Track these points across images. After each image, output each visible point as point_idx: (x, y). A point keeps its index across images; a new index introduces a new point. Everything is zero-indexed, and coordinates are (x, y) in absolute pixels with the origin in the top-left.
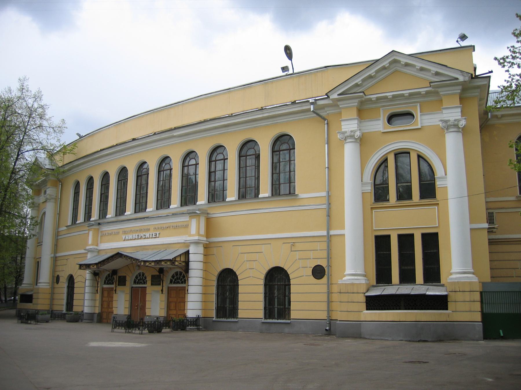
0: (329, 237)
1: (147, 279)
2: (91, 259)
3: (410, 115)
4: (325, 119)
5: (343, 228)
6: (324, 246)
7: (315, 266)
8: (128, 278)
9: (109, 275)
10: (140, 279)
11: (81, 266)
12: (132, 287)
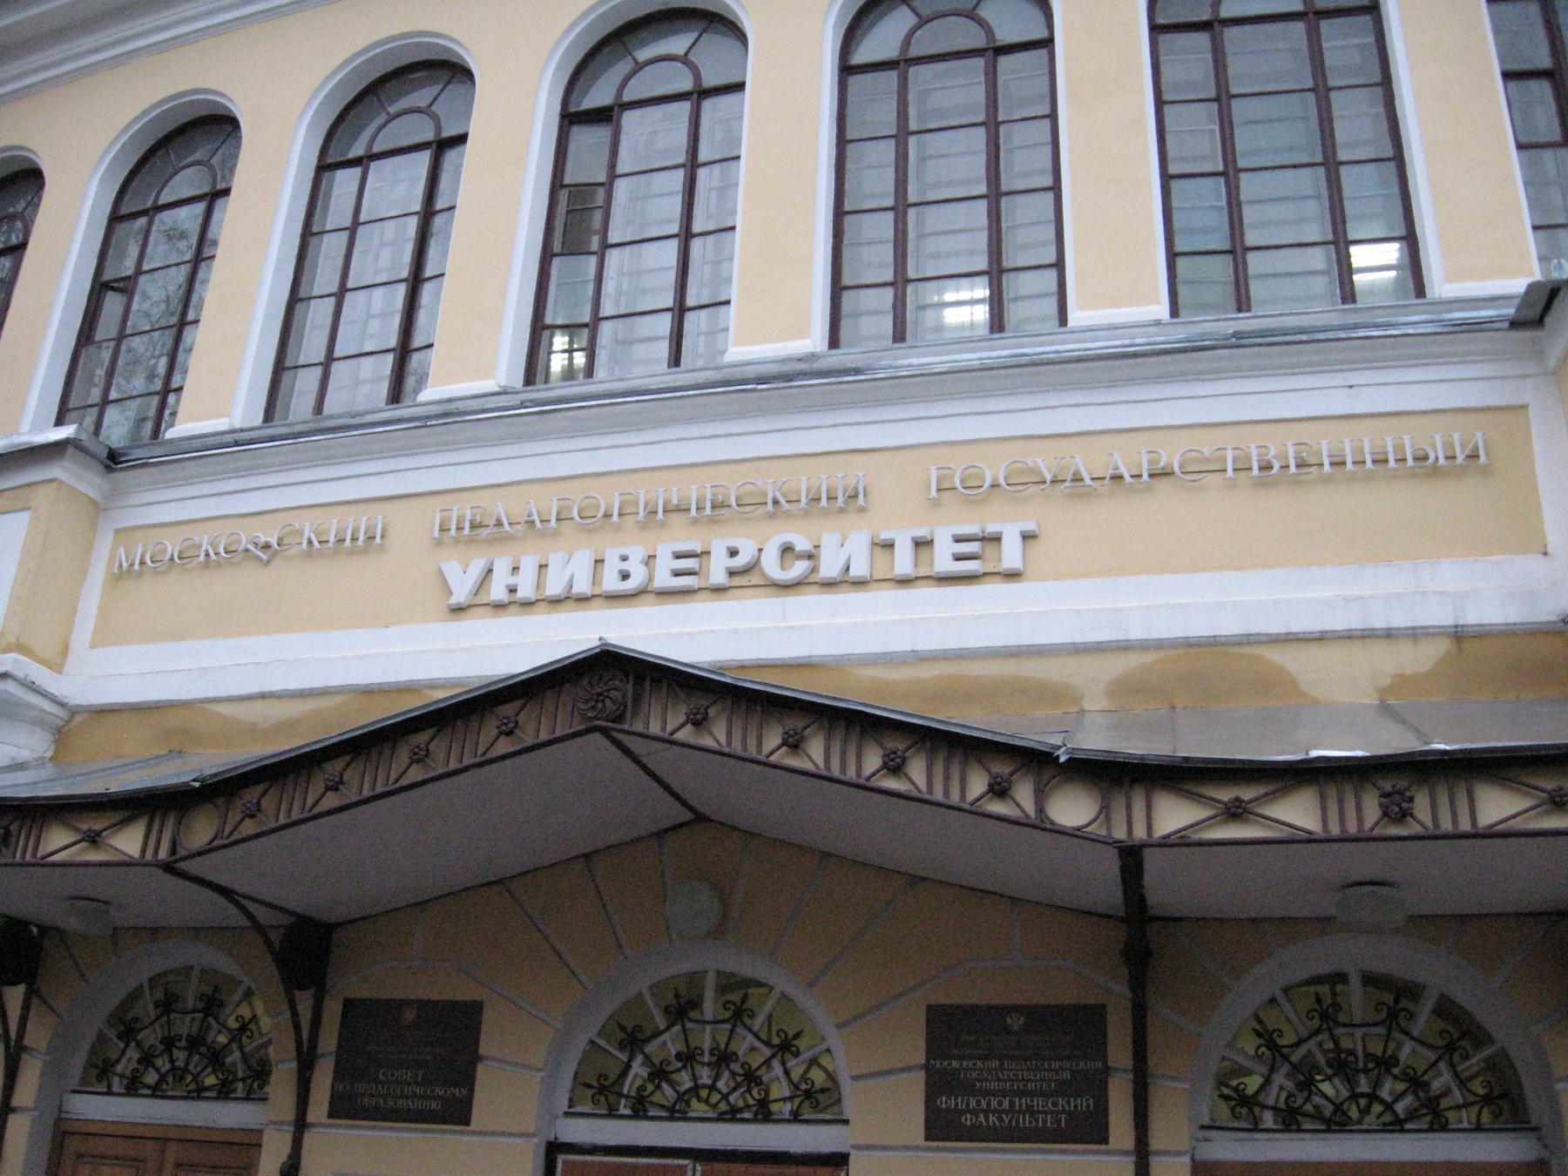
12: (554, 1149)
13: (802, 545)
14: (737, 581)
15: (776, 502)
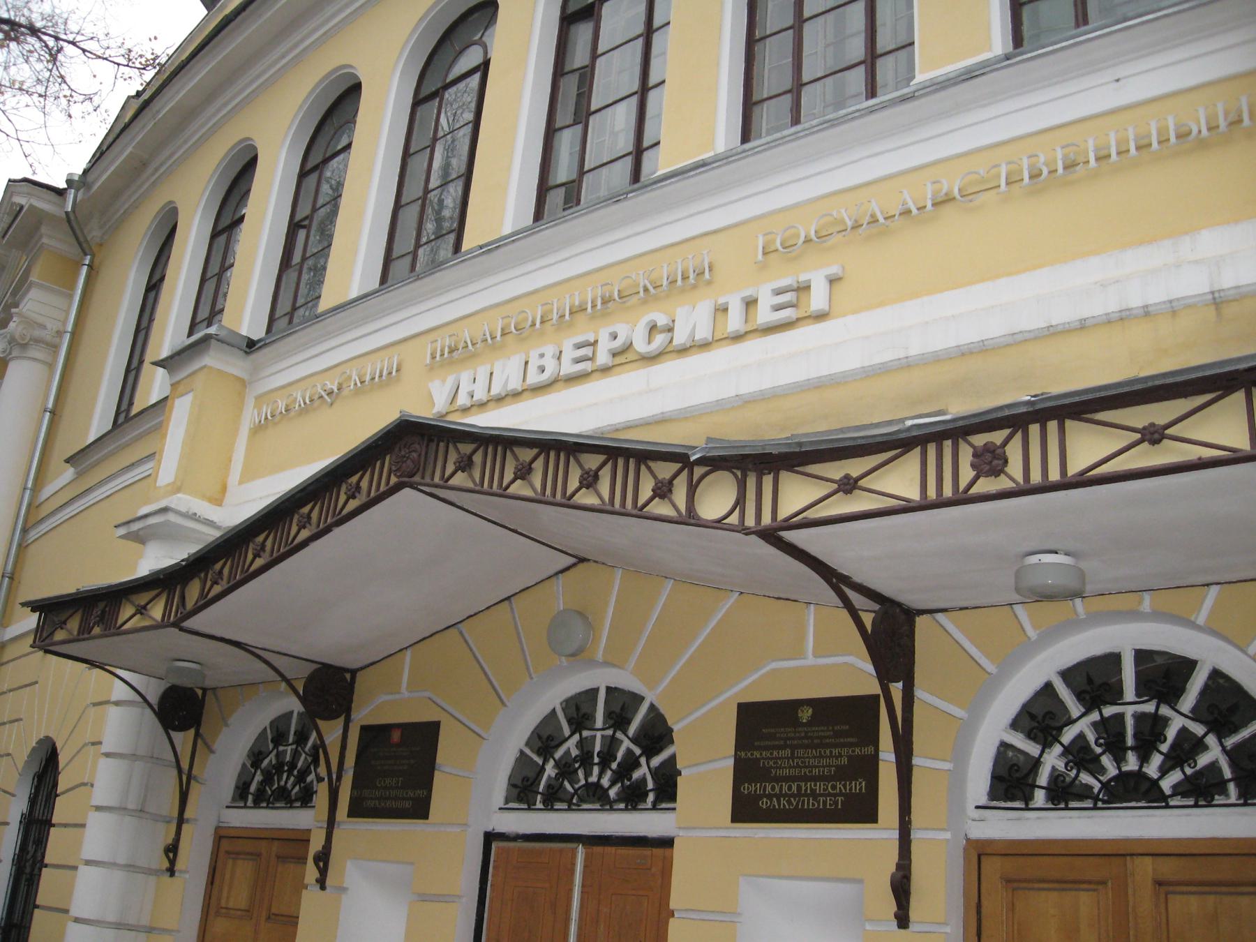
1: (681, 749)
9: (278, 730)
13: (662, 320)
14: (618, 360)
15: (646, 290)
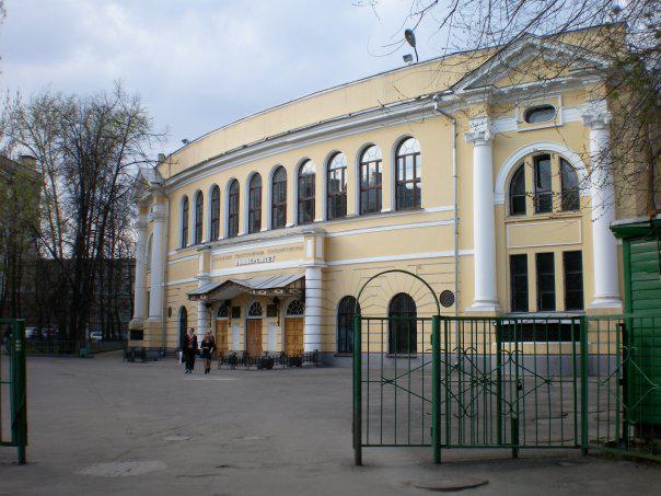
0: (458, 258)
2: (201, 287)
3: (549, 109)
4: (452, 118)
5: (472, 247)
6: (452, 268)
7: (400, 294)
8: (242, 310)
10: (255, 310)
11: (190, 296)
